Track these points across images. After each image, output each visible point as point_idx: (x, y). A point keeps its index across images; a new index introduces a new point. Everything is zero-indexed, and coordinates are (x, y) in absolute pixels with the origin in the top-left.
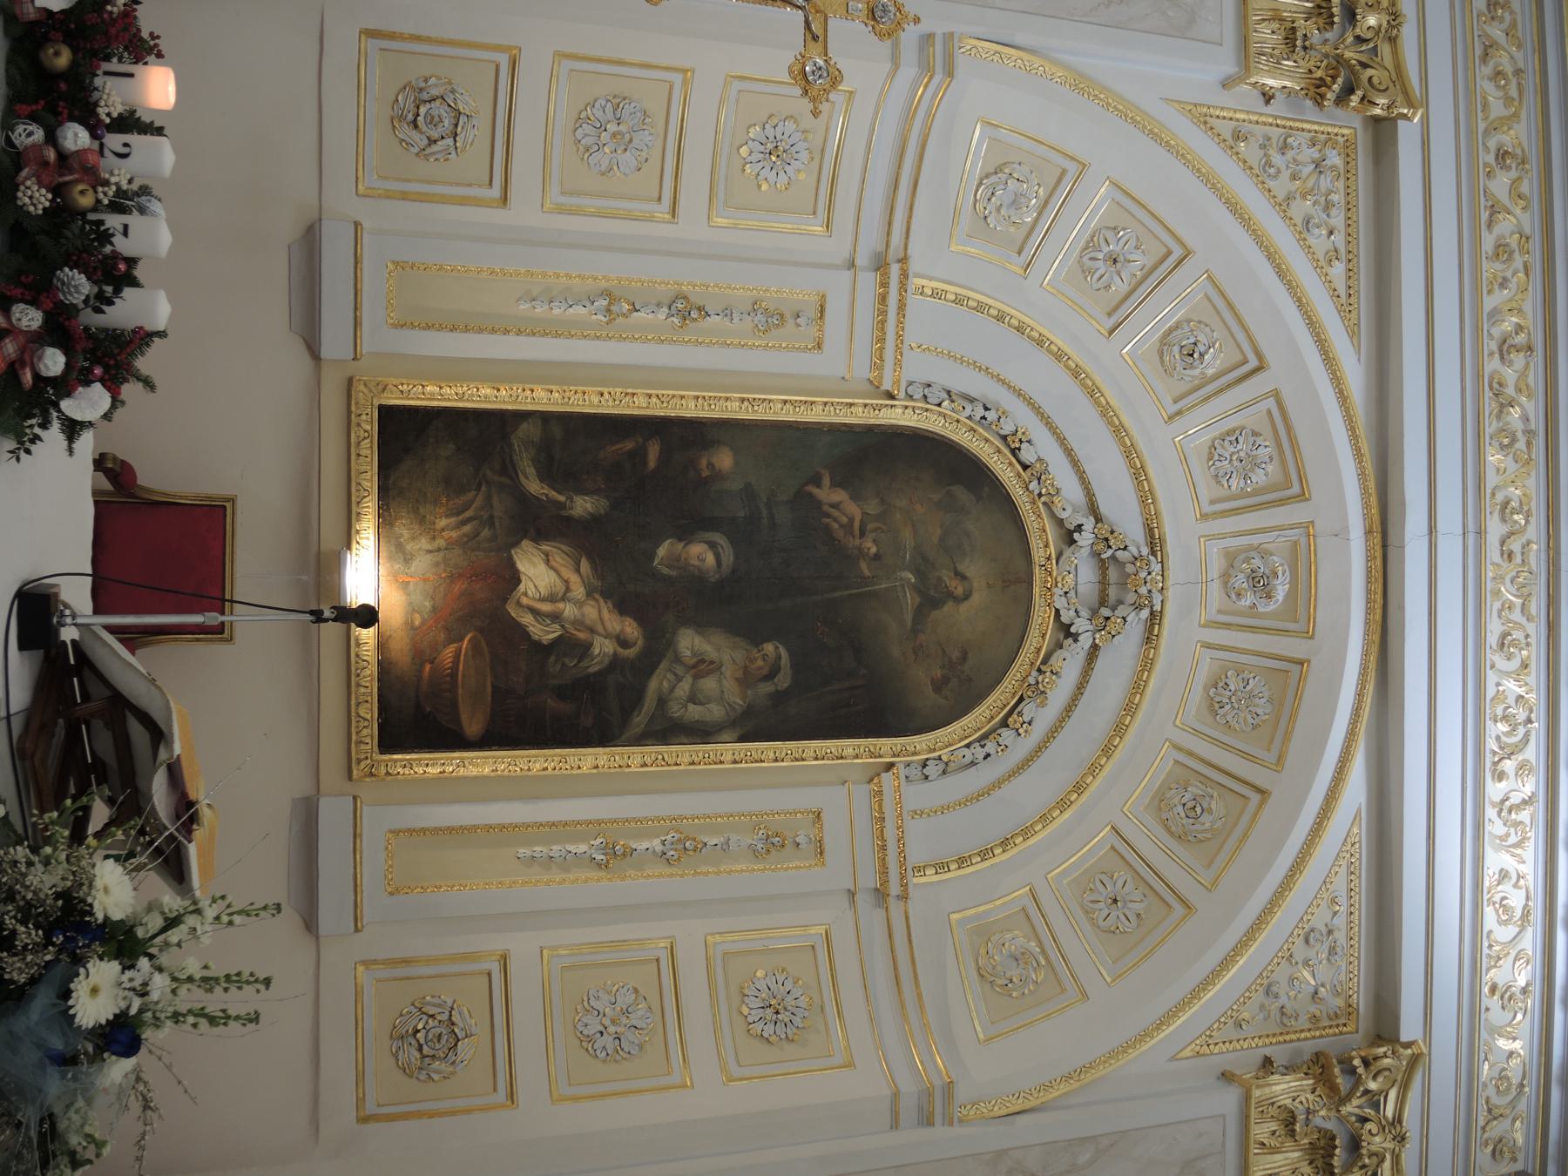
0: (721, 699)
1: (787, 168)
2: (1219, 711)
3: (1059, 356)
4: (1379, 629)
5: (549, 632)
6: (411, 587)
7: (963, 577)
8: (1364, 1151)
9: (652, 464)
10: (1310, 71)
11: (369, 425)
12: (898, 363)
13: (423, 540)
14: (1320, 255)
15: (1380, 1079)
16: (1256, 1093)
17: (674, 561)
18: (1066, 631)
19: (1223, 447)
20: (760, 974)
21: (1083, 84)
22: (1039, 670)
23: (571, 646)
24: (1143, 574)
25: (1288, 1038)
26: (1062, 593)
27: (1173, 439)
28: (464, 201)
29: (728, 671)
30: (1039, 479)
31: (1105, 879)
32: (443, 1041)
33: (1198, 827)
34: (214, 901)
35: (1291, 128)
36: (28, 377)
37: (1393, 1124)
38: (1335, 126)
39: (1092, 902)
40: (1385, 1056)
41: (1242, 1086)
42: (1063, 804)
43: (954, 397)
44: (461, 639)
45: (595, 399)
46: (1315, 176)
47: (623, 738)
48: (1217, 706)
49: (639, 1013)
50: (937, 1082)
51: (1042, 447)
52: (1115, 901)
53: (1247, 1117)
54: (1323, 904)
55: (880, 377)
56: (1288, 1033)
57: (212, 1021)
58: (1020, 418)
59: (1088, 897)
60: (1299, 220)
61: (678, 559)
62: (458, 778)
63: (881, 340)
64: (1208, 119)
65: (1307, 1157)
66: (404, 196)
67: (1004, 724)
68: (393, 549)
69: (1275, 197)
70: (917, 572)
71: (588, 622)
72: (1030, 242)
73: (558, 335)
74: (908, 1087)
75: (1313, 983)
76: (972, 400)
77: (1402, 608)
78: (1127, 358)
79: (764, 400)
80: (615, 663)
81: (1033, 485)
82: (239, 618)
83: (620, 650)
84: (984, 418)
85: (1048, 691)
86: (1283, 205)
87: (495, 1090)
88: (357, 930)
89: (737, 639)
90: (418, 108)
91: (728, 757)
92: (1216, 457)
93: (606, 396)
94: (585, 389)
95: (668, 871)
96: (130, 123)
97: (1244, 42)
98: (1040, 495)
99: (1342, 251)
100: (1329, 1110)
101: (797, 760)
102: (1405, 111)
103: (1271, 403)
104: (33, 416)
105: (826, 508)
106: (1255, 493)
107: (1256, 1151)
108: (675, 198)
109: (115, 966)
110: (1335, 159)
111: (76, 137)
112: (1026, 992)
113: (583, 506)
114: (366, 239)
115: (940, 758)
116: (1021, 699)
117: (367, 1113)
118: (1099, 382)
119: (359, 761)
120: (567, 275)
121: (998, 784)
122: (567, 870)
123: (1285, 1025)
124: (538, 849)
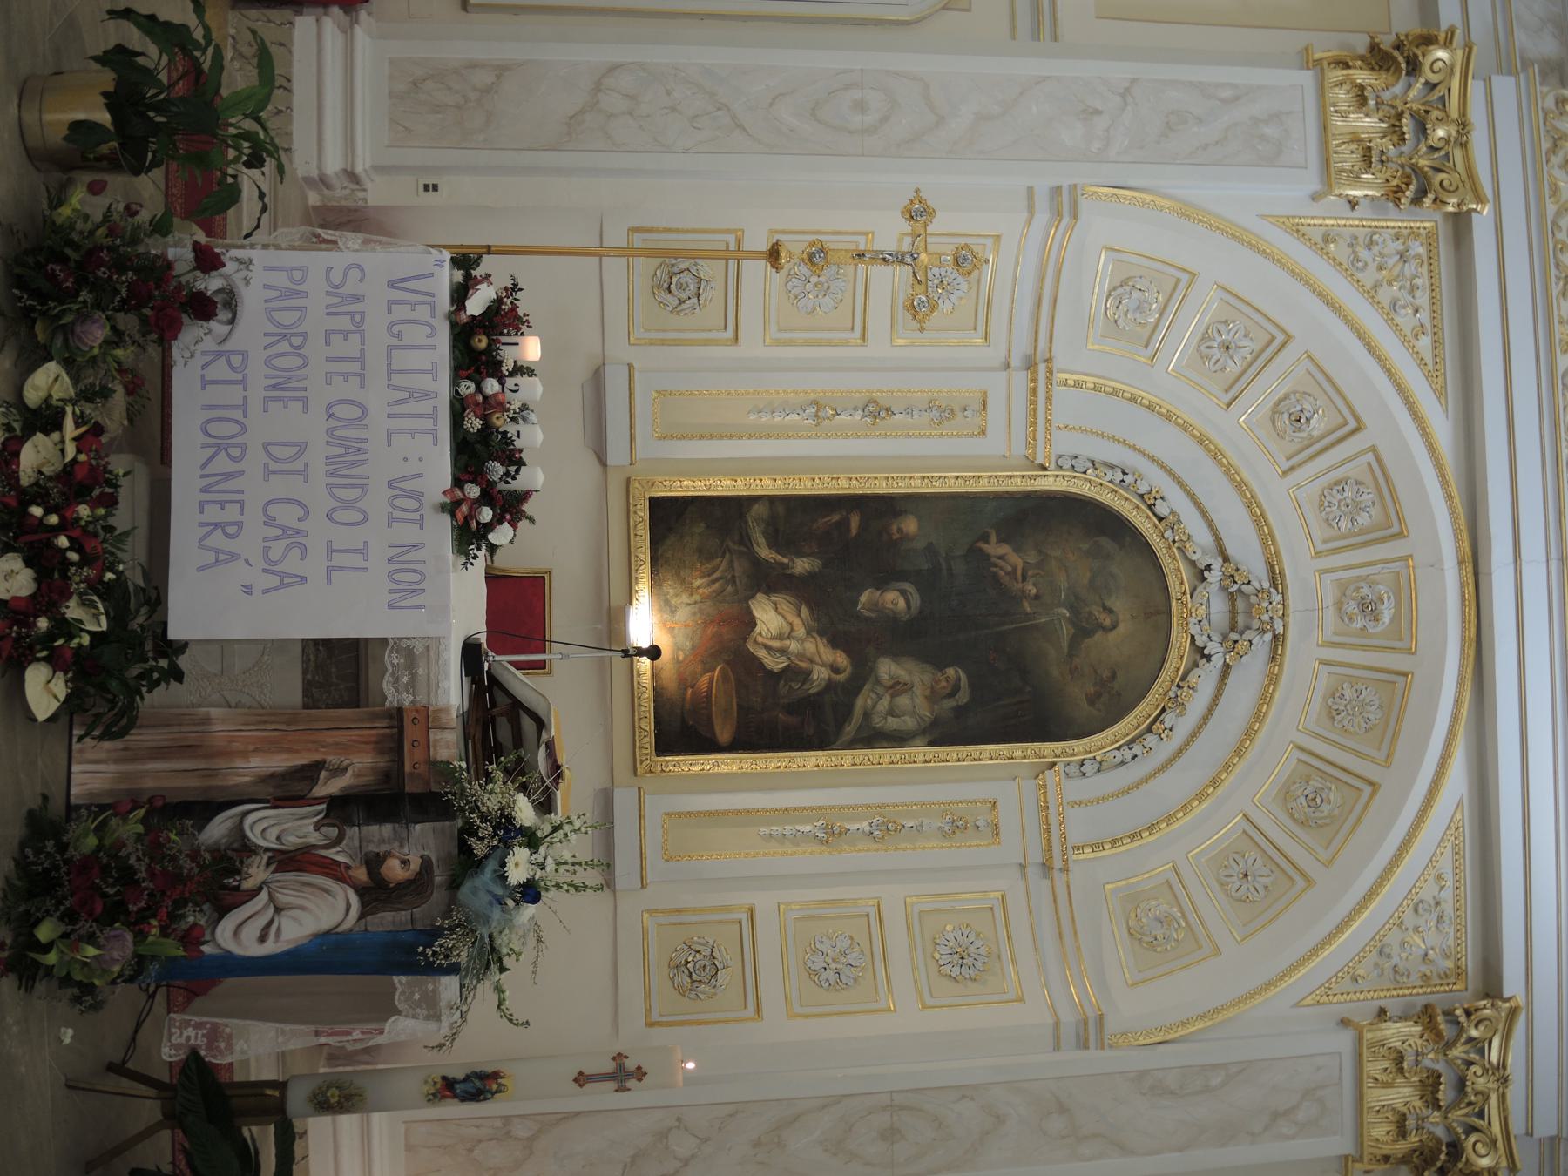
0: (913, 713)
1: (951, 297)
2: (1337, 717)
3: (1185, 427)
4: (1474, 644)
5: (778, 663)
6: (676, 631)
7: (1111, 611)
8: (1469, 1089)
9: (854, 531)
10: (1387, 181)
11: (643, 512)
12: (1048, 442)
13: (684, 596)
14: (1407, 331)
15: (1481, 1028)
16: (1368, 1036)
17: (874, 606)
18: (1201, 654)
19: (1330, 494)
20: (949, 928)
21: (1188, 212)
22: (1179, 687)
23: (795, 673)
24: (1265, 604)
25: (1401, 992)
26: (1196, 621)
27: (1288, 490)
28: (707, 343)
29: (918, 690)
30: (1173, 529)
31: (1236, 856)
32: (707, 970)
33: (1317, 814)
34: (579, 817)
35: (1376, 227)
36: (474, 525)
37: (1498, 1068)
38: (1417, 221)
39: (1227, 876)
40: (1485, 1007)
41: (1356, 1029)
42: (1201, 796)
43: (1097, 466)
44: (714, 670)
45: (809, 484)
46: (1400, 265)
47: (838, 743)
48: (1335, 713)
49: (854, 955)
50: (1090, 1014)
51: (1175, 501)
52: (1246, 876)
53: (1360, 1055)
54: (1431, 880)
55: (1034, 453)
56: (1401, 988)
57: (577, 888)
58: (1155, 479)
59: (1223, 872)
60: (1386, 303)
61: (876, 604)
62: (714, 774)
63: (1034, 424)
64: (1300, 227)
65: (1418, 1093)
66: (663, 342)
67: (1149, 730)
68: (662, 603)
69: (1363, 286)
70: (1071, 608)
71: (808, 655)
72: (1155, 337)
73: (779, 437)
74: (1068, 1018)
75: (1423, 946)
76: (1112, 467)
77: (1491, 625)
78: (1244, 425)
79: (940, 477)
80: (830, 686)
81: (1168, 534)
82: (552, 655)
83: (833, 676)
84: (1123, 481)
85: (1185, 703)
86: (1371, 294)
87: (746, 1007)
88: (643, 887)
89: (924, 665)
90: (671, 278)
91: (920, 758)
92: (1326, 504)
93: (817, 481)
94: (801, 476)
95: (876, 846)
96: (520, 370)
97: (1326, 163)
98: (1174, 542)
99: (1428, 325)
100: (1436, 1052)
101: (975, 760)
102: (1474, 206)
103: (1370, 457)
104: (473, 544)
105: (994, 560)
106: (1362, 532)
107: (1370, 1085)
108: (864, 327)
109: (527, 852)
110: (1418, 249)
111: (491, 386)
112: (1169, 947)
113: (802, 565)
114: (637, 376)
115: (1094, 759)
116: (1163, 710)
117: (653, 1020)
118: (1221, 445)
119: (642, 762)
120: (784, 391)
121: (1146, 779)
122: (797, 845)
123: (1398, 982)
124: (775, 828)
